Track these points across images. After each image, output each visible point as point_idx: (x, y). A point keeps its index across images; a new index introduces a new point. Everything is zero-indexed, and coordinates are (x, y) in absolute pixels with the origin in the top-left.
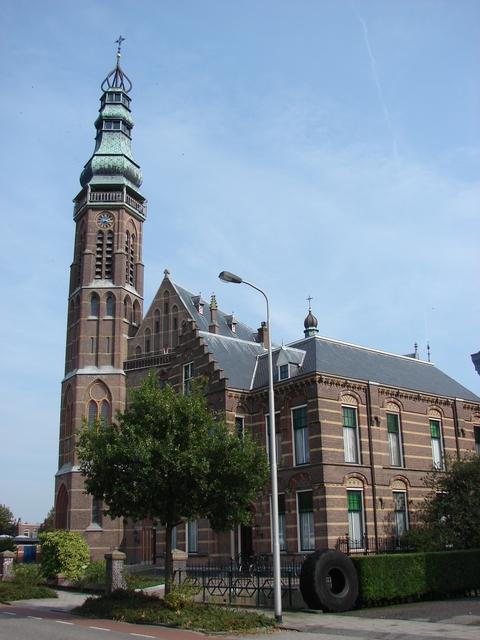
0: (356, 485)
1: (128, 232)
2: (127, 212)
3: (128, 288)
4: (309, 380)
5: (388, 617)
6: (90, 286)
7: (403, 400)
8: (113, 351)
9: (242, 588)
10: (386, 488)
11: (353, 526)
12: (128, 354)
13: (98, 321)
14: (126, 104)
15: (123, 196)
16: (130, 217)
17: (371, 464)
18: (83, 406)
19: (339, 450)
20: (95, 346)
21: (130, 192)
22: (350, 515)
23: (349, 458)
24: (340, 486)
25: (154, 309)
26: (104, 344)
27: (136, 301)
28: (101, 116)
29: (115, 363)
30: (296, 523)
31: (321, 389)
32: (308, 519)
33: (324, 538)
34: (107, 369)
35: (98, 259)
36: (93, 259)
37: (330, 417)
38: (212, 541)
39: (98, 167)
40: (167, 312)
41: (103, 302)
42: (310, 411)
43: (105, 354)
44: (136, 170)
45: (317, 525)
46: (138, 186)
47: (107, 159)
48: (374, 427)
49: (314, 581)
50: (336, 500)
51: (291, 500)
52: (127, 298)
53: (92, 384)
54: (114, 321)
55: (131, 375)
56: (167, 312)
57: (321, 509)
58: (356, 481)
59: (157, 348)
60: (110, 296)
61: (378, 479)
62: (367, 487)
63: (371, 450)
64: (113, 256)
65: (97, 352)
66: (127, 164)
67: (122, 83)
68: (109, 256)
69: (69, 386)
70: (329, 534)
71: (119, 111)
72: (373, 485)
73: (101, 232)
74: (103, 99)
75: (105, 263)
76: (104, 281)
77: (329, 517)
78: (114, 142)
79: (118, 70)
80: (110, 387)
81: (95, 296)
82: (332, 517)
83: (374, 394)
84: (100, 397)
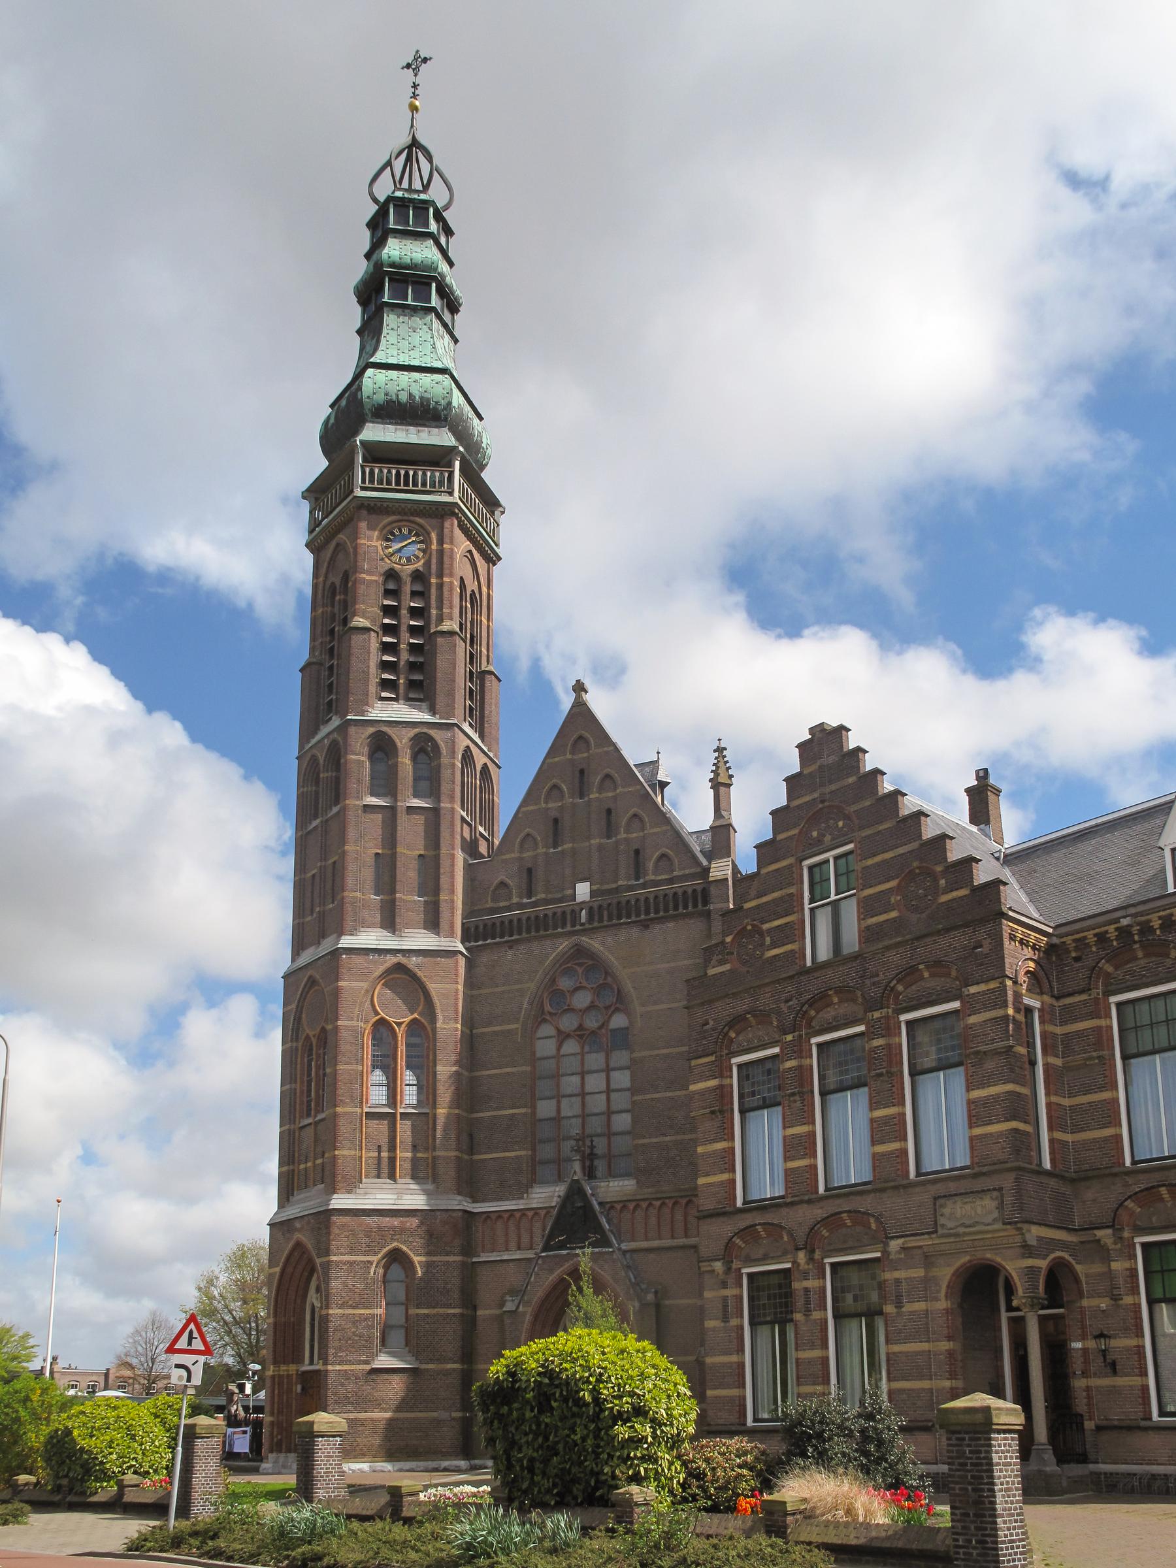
2: (462, 527)
18: (355, 1031)
25: (544, 785)
26: (408, 873)
34: (419, 939)
35: (387, 648)
36: (374, 645)
39: (380, 398)
41: (405, 761)
43: (410, 898)
47: (404, 378)
55: (485, 958)
60: (424, 747)
69: (312, 982)
71: (423, 252)
73: (391, 575)
75: (405, 656)
78: (416, 339)
80: (432, 987)
81: (382, 744)
84: (400, 1016)
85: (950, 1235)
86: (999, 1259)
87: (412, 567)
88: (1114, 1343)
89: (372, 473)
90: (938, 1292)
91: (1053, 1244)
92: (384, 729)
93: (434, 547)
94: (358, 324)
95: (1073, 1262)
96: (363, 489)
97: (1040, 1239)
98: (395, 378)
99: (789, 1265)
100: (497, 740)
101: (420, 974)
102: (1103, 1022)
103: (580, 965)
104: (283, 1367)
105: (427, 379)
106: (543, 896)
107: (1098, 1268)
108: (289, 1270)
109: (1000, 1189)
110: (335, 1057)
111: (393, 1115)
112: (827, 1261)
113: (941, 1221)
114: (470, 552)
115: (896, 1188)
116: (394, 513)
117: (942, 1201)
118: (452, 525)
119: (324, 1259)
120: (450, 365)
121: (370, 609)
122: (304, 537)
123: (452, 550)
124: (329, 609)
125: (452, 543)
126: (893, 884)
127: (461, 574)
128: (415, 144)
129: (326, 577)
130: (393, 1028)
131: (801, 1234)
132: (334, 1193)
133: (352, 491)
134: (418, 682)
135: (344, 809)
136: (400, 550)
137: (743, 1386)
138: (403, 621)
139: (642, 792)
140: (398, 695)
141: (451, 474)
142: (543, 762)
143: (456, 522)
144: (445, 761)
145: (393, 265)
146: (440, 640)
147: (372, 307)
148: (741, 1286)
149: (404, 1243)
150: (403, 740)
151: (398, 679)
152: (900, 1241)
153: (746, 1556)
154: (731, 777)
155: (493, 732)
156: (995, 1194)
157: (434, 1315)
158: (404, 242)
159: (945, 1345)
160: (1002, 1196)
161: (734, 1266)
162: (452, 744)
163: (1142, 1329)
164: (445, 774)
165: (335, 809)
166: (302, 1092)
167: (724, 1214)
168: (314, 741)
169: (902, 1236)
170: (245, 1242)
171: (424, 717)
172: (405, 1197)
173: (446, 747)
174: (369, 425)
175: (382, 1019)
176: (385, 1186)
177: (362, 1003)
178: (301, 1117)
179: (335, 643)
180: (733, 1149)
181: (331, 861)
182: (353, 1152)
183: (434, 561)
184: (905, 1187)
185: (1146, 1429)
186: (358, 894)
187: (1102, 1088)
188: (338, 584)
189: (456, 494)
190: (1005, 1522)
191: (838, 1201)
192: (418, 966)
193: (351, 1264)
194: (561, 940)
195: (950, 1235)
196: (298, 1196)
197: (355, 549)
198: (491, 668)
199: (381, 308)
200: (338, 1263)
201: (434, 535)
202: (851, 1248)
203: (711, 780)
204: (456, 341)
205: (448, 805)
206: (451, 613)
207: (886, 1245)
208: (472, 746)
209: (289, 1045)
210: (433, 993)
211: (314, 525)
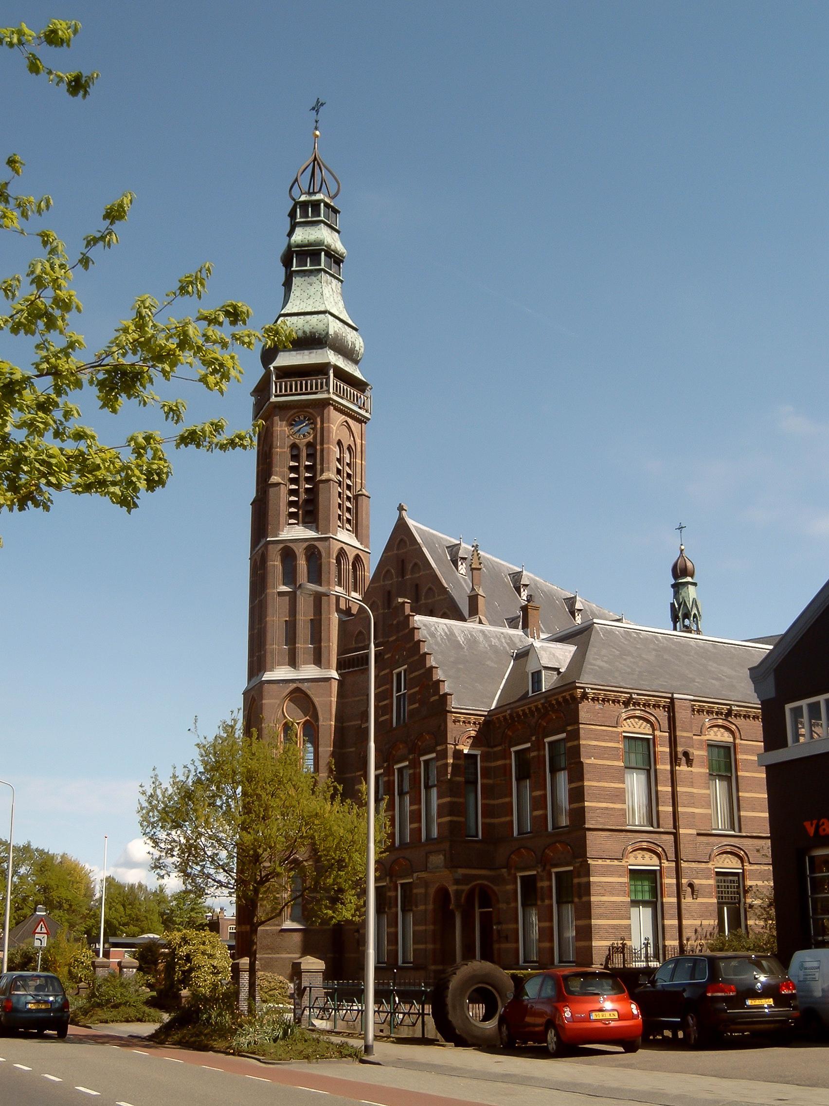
0: (648, 862)
1: (339, 443)
2: (336, 409)
4: (567, 695)
5: (569, 1064)
7: (740, 722)
10: (703, 865)
11: (640, 926)
15: (328, 384)
17: (675, 827)
19: (618, 806)
22: (634, 911)
23: (638, 818)
24: (616, 863)
27: (357, 556)
28: (289, 246)
30: (551, 920)
31: (585, 710)
32: (569, 911)
34: (309, 671)
35: (292, 492)
36: (283, 491)
37: (603, 753)
41: (302, 563)
42: (569, 744)
43: (304, 645)
48: (683, 768)
49: (446, 1005)
50: (608, 885)
51: (545, 884)
52: (342, 553)
58: (648, 855)
60: (313, 553)
61: (685, 851)
62: (666, 864)
63: (675, 805)
67: (323, 180)
72: (677, 861)
73: (294, 446)
74: (292, 215)
75: (303, 496)
77: (594, 911)
78: (312, 290)
80: (316, 700)
81: (288, 553)
82: (601, 911)
83: (682, 714)
88: (504, 926)
93: (319, 426)
95: (492, 886)
96: (276, 396)
100: (368, 537)
101: (309, 692)
102: (508, 762)
105: (314, 319)
106: (381, 640)
114: (346, 422)
116: (295, 408)
118: (329, 411)
126: (417, 689)
128: (315, 159)
134: (309, 511)
136: (299, 430)
144: (324, 560)
145: (298, 246)
150: (300, 551)
153: (285, 1033)
158: (306, 228)
171: (311, 534)
183: (319, 435)
187: (505, 796)
192: (308, 688)
201: (319, 420)
208: (345, 546)
210: (317, 704)
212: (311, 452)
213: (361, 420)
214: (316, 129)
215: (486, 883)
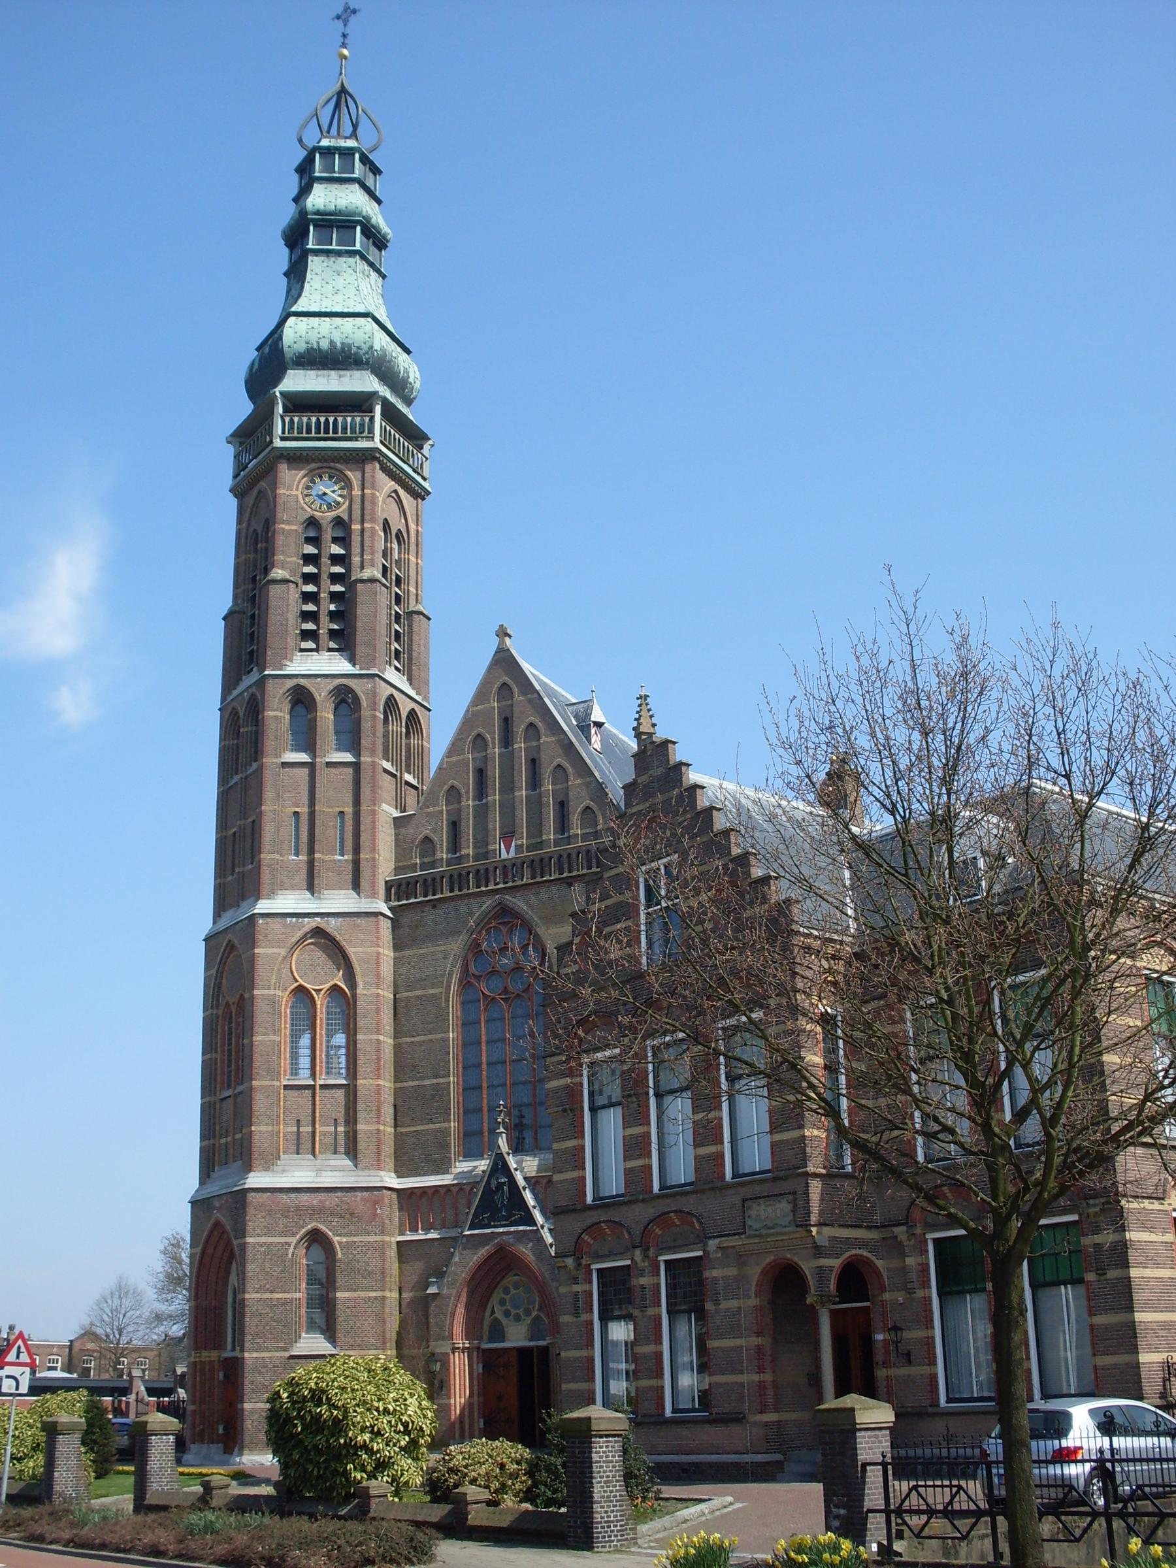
1: (386, 526)
2: (384, 469)
3: (391, 675)
6: (289, 670)
8: (357, 850)
9: (931, 1512)
12: (397, 860)
13: (311, 766)
14: (370, 183)
16: (392, 485)
18: (274, 1002)
20: (304, 837)
21: (391, 414)
25: (470, 735)
26: (329, 831)
27: (412, 713)
29: (364, 883)
33: (1123, 1359)
34: (340, 900)
35: (307, 597)
36: (293, 594)
38: (756, 1377)
39: (301, 347)
40: (507, 740)
41: (326, 715)
43: (334, 858)
44: (403, 361)
45: (1099, 1320)
46: (409, 402)
47: (326, 324)
53: (304, 937)
54: (356, 766)
55: (407, 919)
56: (507, 740)
57: (1112, 1274)
59: (482, 841)
60: (345, 698)
64: (351, 586)
65: (311, 851)
66: (381, 341)
68: (338, 588)
69: (231, 947)
70: (1142, 1344)
71: (349, 198)
73: (312, 522)
76: (326, 655)
77: (1138, 1296)
78: (340, 282)
79: (343, 91)
80: (351, 951)
81: (301, 699)
84: (322, 977)
85: (756, 1236)
86: (796, 1259)
87: (333, 514)
88: (906, 1335)
89: (292, 421)
90: (749, 1289)
91: (849, 1243)
92: (302, 681)
94: (285, 268)
95: (873, 1258)
96: (282, 439)
97: (832, 1239)
98: (316, 326)
99: (628, 1262)
100: (427, 684)
101: (339, 938)
103: (504, 924)
104: (205, 1354)
107: (896, 1263)
108: (210, 1251)
109: (795, 1193)
110: (252, 1028)
111: (312, 1087)
112: (661, 1258)
113: (749, 1222)
114: (396, 491)
115: (713, 1189)
116: (314, 461)
117: (750, 1203)
118: (374, 471)
119: (239, 1241)
120: (372, 309)
121: (289, 559)
122: (229, 481)
123: (373, 494)
124: (252, 556)
125: (373, 488)
127: (385, 516)
129: (249, 524)
130: (313, 998)
131: (637, 1231)
132: (250, 1171)
133: (271, 442)
135: (261, 769)
137: (593, 1379)
138: (323, 569)
139: (566, 742)
140: (318, 645)
141: (372, 419)
142: (467, 711)
143: (377, 466)
144: (365, 713)
145: (318, 212)
146: (359, 586)
147: (298, 251)
148: (591, 1282)
149: (323, 1223)
150: (322, 694)
151: (318, 629)
152: (717, 1241)
154: (654, 725)
155: (422, 674)
156: (791, 1197)
157: (355, 1299)
159: (755, 1341)
160: (795, 1200)
161: (584, 1262)
162: (374, 694)
163: (932, 1321)
164: (366, 726)
165: (255, 765)
166: (223, 1062)
167: (575, 1210)
168: (235, 693)
169: (718, 1237)
170: (1003, 649)
172: (324, 1173)
173: (367, 699)
174: (290, 372)
175: (301, 986)
176: (303, 1163)
177: (281, 971)
178: (222, 1088)
179: (256, 591)
180: (583, 1147)
181: (250, 820)
182: (270, 1128)
184: (721, 1189)
185: (934, 1415)
186: (275, 856)
188: (259, 531)
189: (377, 438)
190: (602, 1507)
191: (667, 1201)
192: (338, 929)
193: (268, 1245)
194: (484, 899)
195: (756, 1236)
196: (218, 1172)
197: (275, 497)
198: (420, 608)
199: (306, 253)
200: (254, 1245)
202: (680, 1246)
203: (634, 729)
204: (384, 277)
205: (369, 759)
206: (372, 559)
207: (705, 1245)
208: (396, 694)
209: (210, 1011)
210: (353, 958)
211: (240, 467)
212: (341, 535)
213: (419, 494)
214: (344, 45)
215: (865, 1253)
